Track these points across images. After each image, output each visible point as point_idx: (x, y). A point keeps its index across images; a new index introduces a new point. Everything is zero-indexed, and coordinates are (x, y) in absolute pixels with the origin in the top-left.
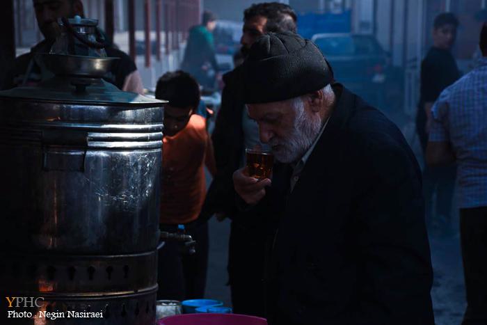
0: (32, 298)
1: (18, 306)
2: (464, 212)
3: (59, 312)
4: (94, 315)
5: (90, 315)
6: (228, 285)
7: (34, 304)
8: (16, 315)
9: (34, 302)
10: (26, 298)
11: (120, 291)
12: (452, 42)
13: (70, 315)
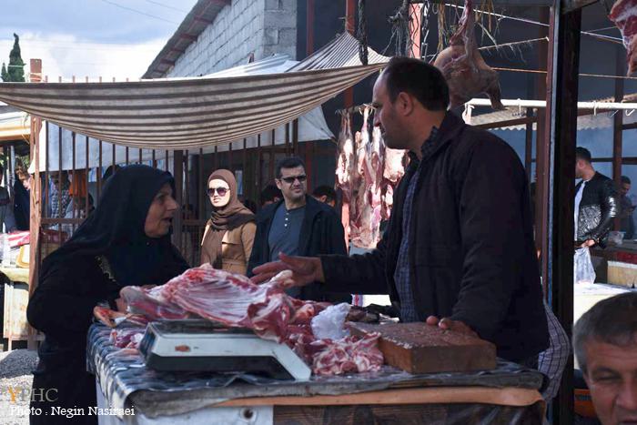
0: (42, 390)
2: (13, 342)
3: (77, 408)
6: (38, 334)
7: (44, 398)
9: (44, 395)
13: (92, 412)
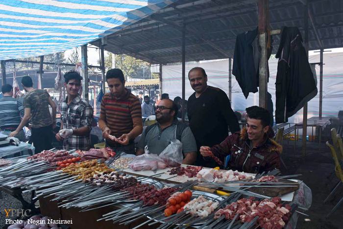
1: (12, 216)
4: (66, 222)
5: (63, 222)
8: (11, 222)
10: (18, 210)
11: (284, 112)
12: (92, 43)
